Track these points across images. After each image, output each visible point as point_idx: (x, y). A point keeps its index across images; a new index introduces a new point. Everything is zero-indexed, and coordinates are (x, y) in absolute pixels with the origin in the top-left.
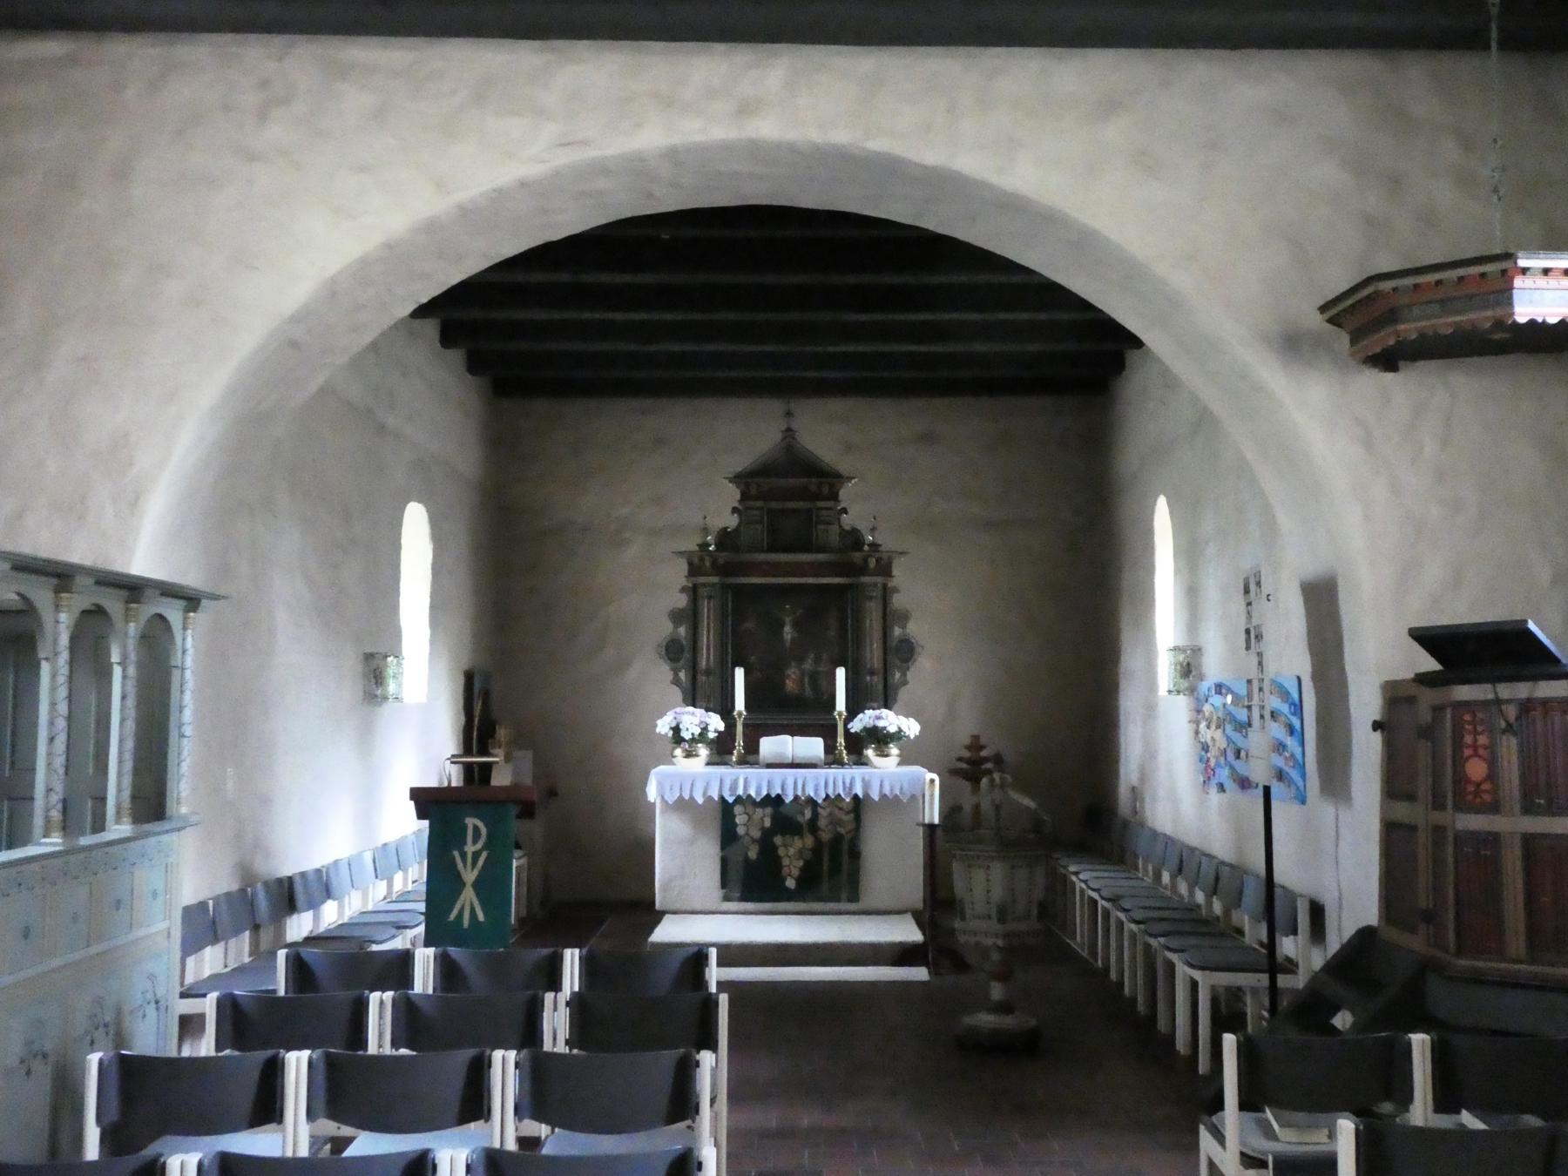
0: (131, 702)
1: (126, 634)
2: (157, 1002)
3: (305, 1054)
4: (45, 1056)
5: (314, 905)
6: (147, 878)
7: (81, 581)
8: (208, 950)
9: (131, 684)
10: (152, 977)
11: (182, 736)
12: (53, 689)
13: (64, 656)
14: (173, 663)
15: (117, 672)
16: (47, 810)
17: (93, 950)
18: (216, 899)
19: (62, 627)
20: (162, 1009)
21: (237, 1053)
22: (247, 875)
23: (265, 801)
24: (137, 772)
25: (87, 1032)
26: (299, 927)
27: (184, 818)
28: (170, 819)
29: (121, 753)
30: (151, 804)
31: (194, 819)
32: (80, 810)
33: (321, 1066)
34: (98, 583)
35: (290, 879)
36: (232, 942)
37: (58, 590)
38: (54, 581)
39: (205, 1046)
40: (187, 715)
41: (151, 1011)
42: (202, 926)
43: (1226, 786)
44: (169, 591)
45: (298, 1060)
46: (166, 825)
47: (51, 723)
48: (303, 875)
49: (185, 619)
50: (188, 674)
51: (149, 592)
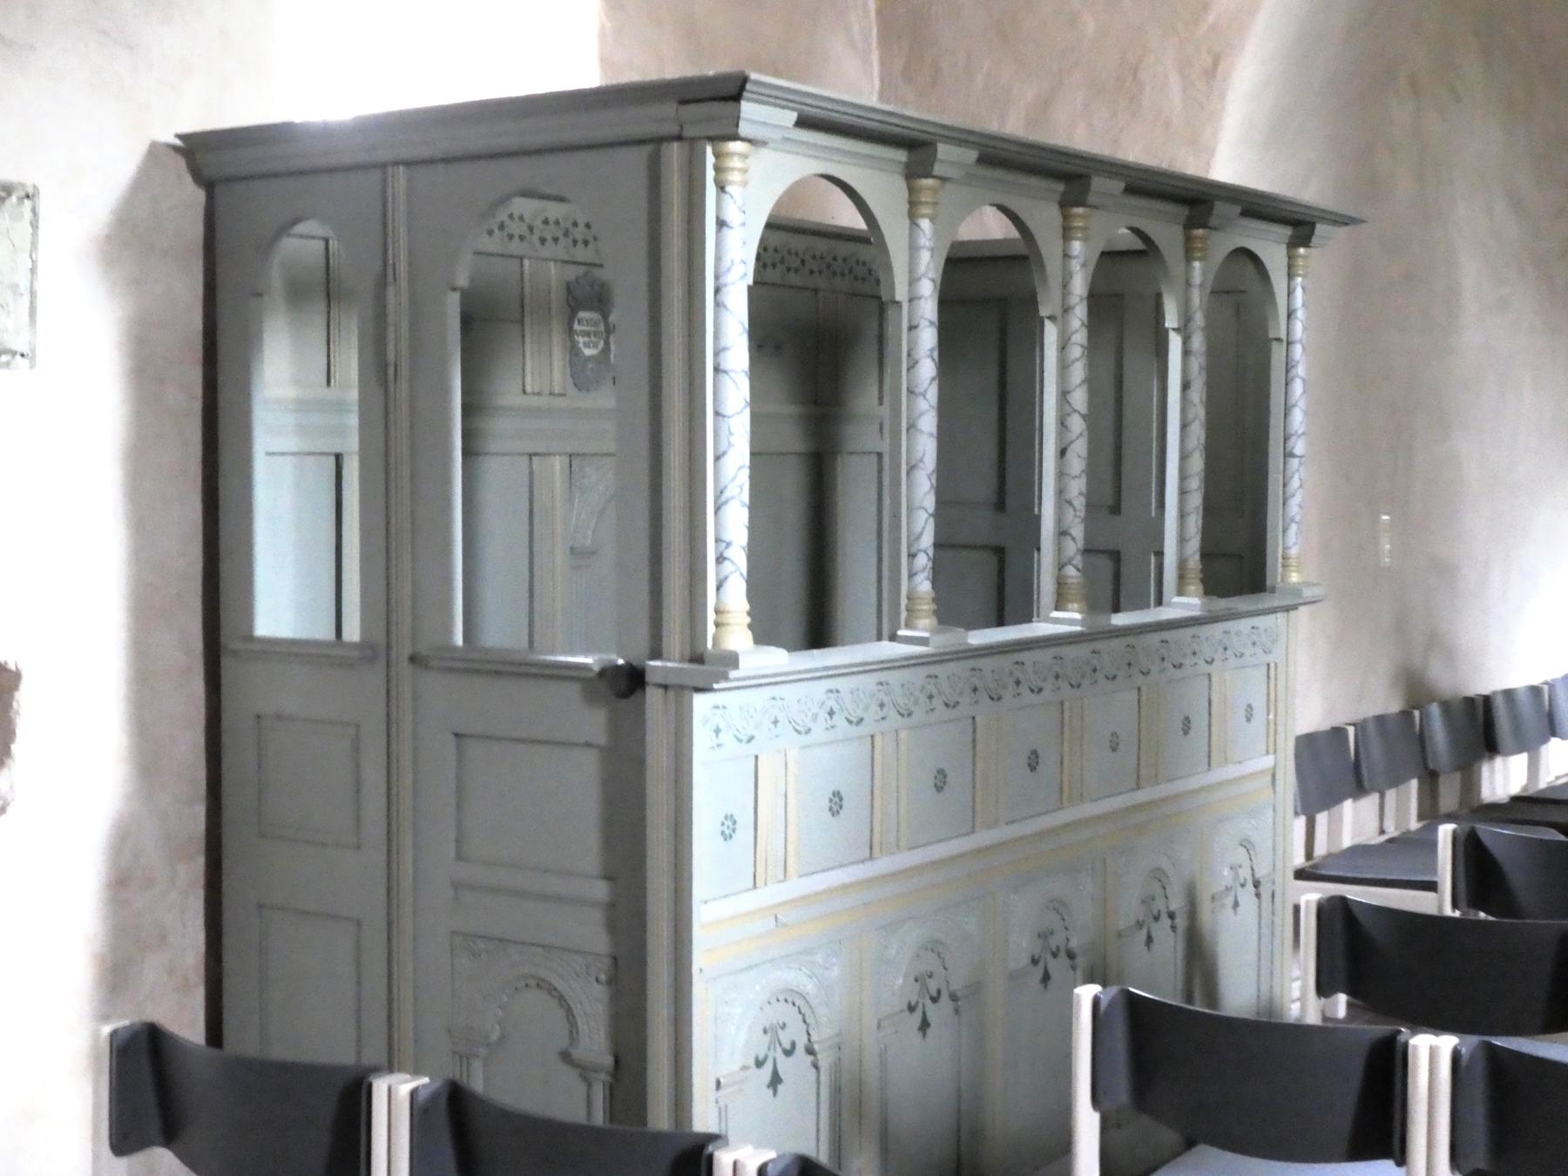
0: (1197, 394)
1: (1188, 284)
2: (1257, 884)
3: (1447, 1043)
4: (1071, 955)
5: (1529, 744)
6: (1237, 684)
7: (1100, 185)
8: (1348, 805)
9: (1196, 363)
10: (1246, 844)
11: (1288, 455)
12: (1064, 366)
13: (1080, 313)
14: (1272, 335)
15: (1175, 343)
16: (1061, 567)
17: (1141, 796)
18: (1360, 726)
19: (1076, 266)
20: (1266, 895)
21: (1491, 918)
22: (1416, 692)
23: (1444, 572)
24: (1210, 510)
25: (1140, 924)
26: (1505, 778)
27: (1296, 591)
28: (1273, 590)
29: (1183, 477)
30: (1238, 564)
31: (1308, 593)
32: (1116, 573)
33: (1480, 1071)
34: (1131, 190)
35: (1487, 700)
36: (1391, 795)
37: (1065, 204)
38: (1060, 187)
39: (1440, 903)
40: (1298, 418)
41: (1247, 896)
42: (1331, 768)
43: (1242, 713)
44: (1256, 207)
45: (1433, 1052)
46: (1266, 601)
47: (1062, 424)
48: (1509, 694)
49: (1291, 257)
50: (1298, 351)
51: (1220, 208)
